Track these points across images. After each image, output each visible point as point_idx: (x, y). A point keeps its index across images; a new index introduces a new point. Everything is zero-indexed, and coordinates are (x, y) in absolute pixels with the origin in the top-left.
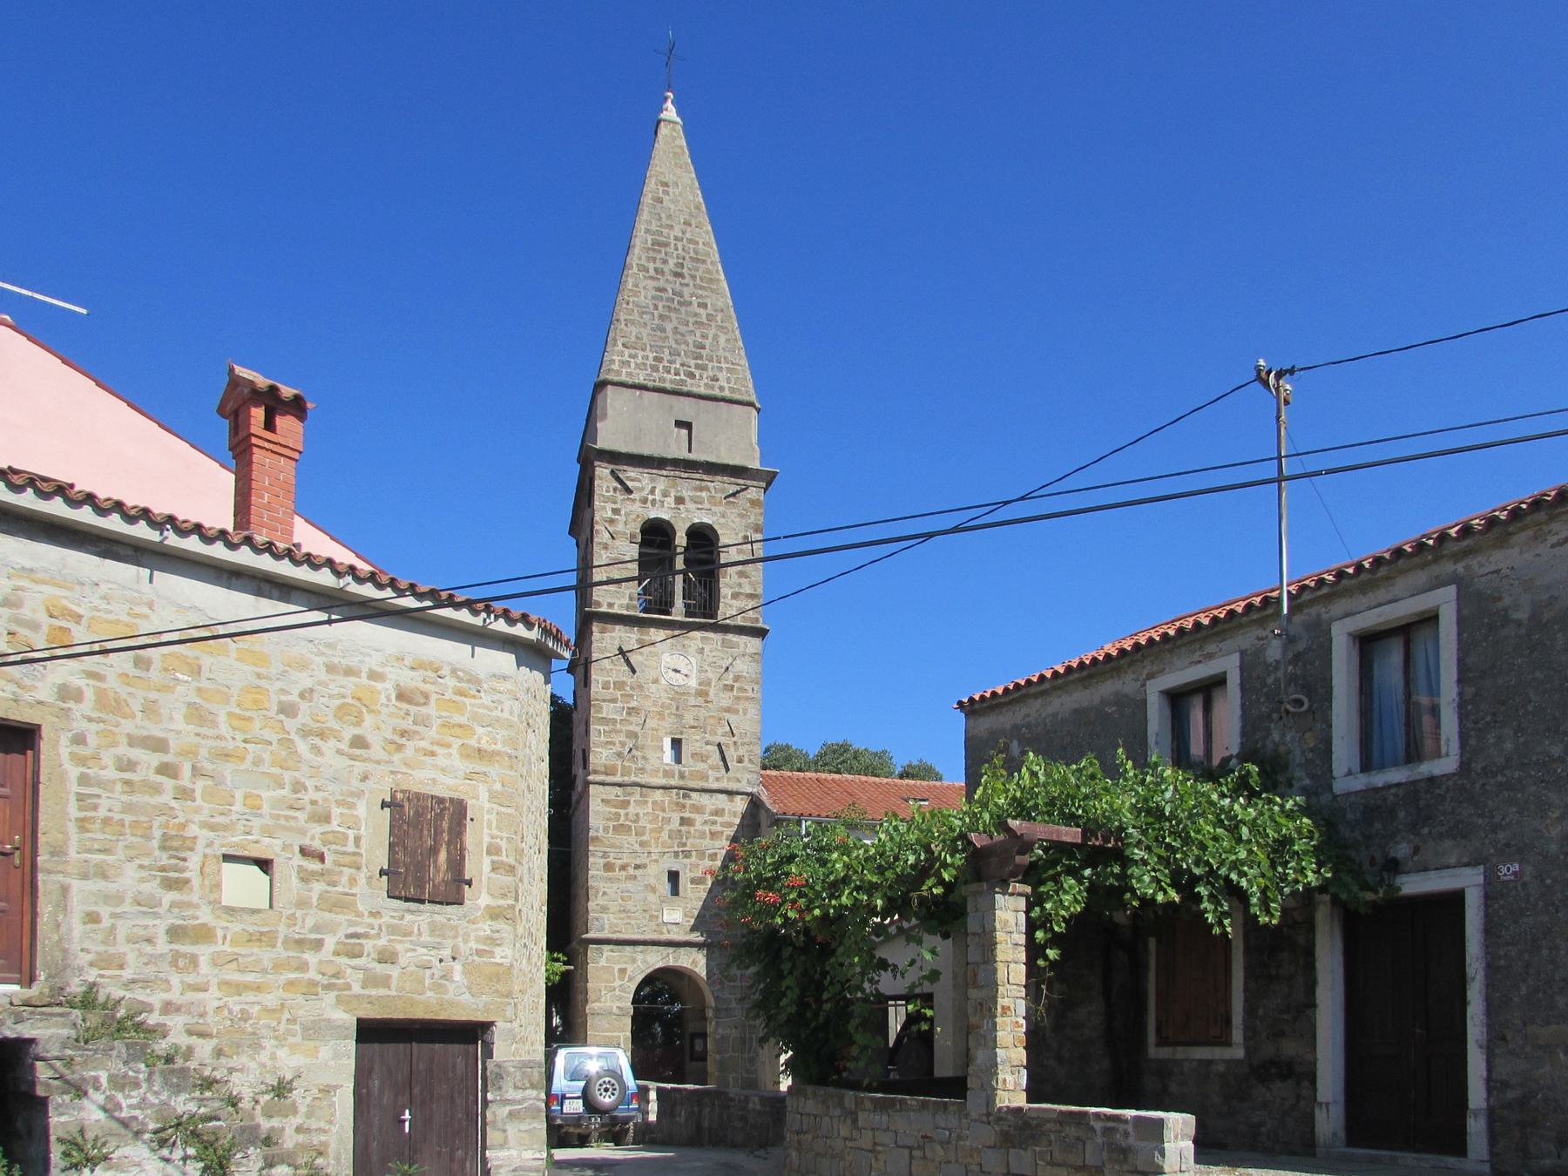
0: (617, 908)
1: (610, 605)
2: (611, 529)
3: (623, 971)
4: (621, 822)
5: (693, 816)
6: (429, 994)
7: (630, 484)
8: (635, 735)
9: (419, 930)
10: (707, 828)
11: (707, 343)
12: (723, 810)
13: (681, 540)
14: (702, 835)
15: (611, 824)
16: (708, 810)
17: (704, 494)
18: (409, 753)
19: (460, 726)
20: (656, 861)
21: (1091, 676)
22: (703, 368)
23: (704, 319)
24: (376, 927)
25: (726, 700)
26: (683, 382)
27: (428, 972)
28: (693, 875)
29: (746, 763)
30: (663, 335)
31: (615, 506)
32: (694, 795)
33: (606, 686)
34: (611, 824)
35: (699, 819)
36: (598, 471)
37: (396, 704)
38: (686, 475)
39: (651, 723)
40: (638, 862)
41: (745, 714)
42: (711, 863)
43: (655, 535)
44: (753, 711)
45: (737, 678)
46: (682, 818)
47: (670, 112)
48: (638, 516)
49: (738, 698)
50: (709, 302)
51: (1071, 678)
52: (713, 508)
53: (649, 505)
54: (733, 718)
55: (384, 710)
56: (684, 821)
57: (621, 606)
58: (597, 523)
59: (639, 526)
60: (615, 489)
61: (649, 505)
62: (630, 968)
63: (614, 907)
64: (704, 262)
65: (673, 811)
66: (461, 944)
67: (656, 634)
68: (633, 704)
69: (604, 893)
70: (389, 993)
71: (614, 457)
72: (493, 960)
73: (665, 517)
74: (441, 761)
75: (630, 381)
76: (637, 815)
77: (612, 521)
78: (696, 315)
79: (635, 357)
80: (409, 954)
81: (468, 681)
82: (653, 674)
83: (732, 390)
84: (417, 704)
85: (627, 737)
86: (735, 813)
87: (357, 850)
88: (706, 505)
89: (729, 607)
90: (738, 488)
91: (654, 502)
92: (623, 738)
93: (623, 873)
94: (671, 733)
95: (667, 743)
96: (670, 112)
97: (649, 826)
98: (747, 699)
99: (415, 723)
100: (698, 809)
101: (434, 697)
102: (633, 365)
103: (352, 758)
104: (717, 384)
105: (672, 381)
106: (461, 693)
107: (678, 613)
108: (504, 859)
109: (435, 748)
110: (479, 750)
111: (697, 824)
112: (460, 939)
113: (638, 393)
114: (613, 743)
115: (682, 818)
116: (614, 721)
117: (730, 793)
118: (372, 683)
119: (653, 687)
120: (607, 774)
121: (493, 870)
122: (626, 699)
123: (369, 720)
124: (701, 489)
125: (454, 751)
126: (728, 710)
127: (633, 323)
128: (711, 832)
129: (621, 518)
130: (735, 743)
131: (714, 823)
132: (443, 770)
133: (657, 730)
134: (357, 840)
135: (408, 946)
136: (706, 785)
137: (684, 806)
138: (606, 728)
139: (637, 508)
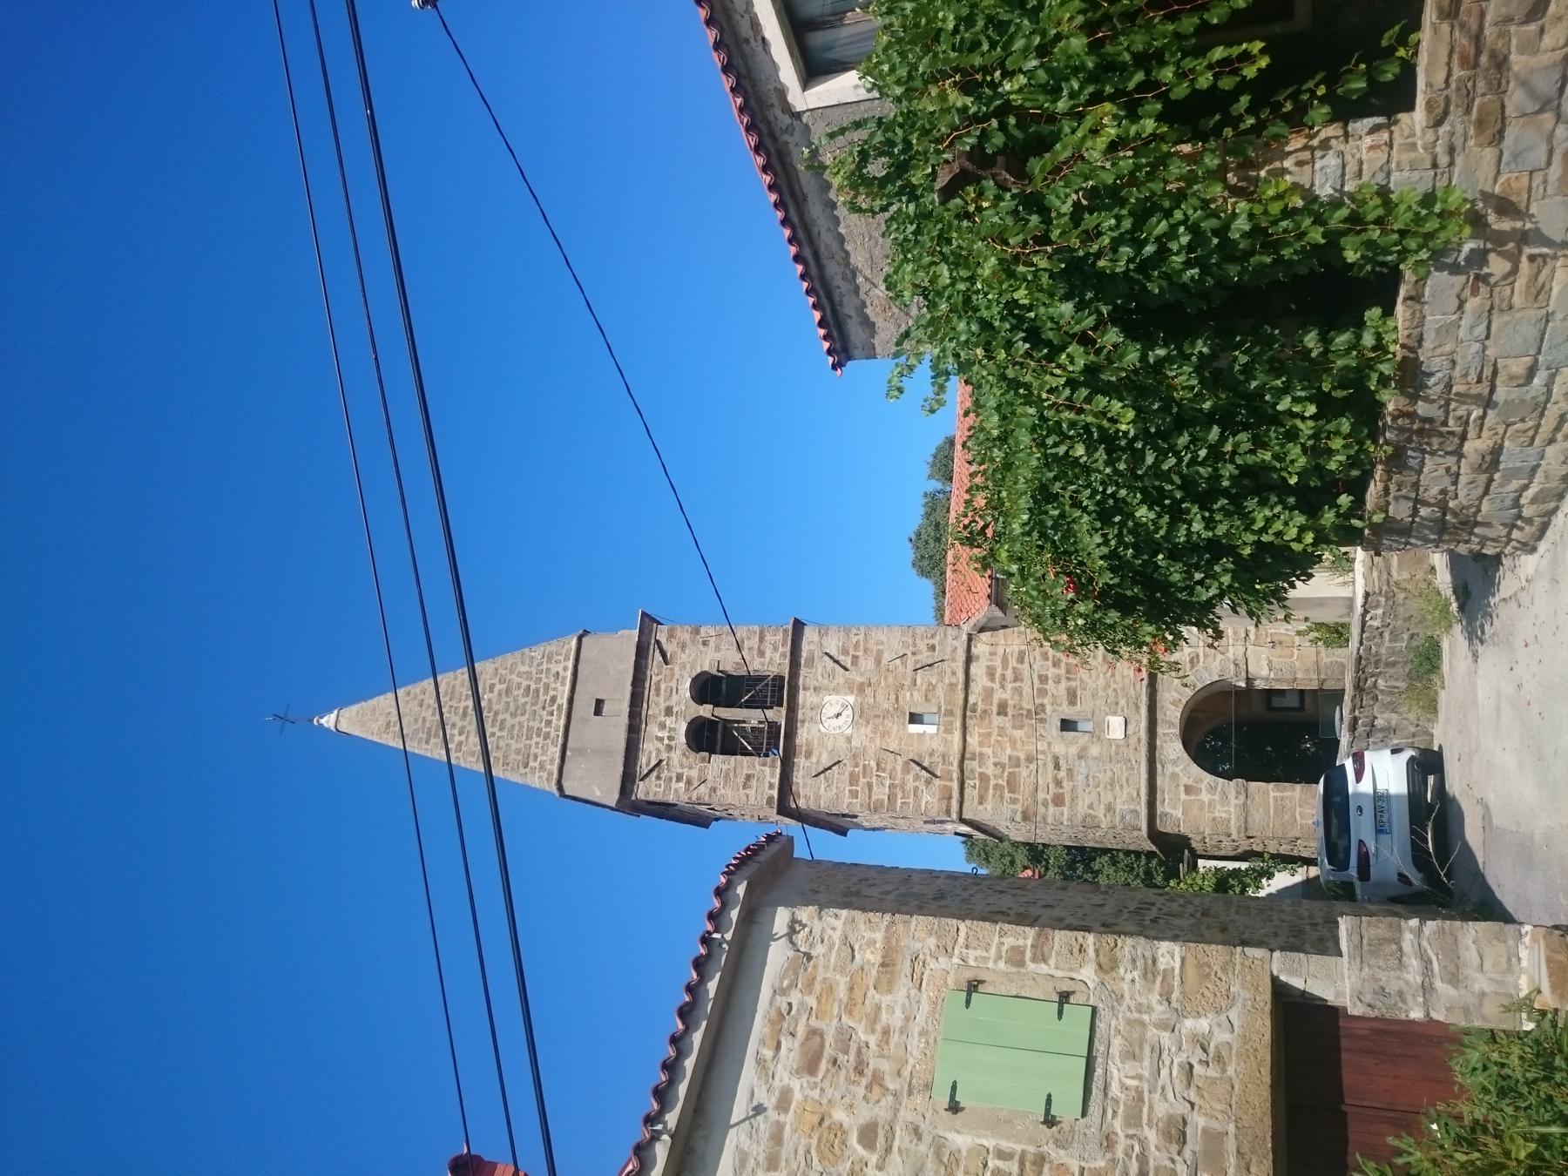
0: (1110, 794)
1: (771, 786)
2: (696, 784)
3: (1188, 790)
4: (1005, 783)
5: (995, 702)
6: (1230, 1071)
7: (653, 763)
8: (906, 764)
9: (1132, 1078)
10: (1009, 686)
11: (525, 683)
12: (988, 667)
13: (706, 711)
14: (1018, 691)
15: (1007, 795)
16: (989, 684)
17: (663, 686)
18: (885, 1066)
19: (851, 989)
20: (1049, 744)
21: (793, 194)
22: (547, 687)
23: (505, 686)
24: (1129, 1142)
25: (867, 664)
26: (560, 707)
27: (1198, 1069)
28: (1065, 703)
29: (935, 641)
30: (517, 728)
31: (674, 779)
32: (972, 700)
33: (854, 794)
34: (1007, 795)
35: (999, 695)
36: (641, 796)
37: (820, 1077)
38: (645, 705)
39: (893, 746)
40: (1051, 765)
41: (883, 643)
42: (1050, 681)
43: (705, 738)
44: (878, 635)
45: (845, 652)
46: (999, 714)
47: (328, 721)
48: (684, 754)
49: (866, 650)
50: (489, 682)
51: (795, 219)
52: (677, 677)
53: (673, 743)
54: (886, 657)
55: (829, 1092)
56: (1002, 710)
57: (772, 775)
58: (690, 798)
59: (693, 754)
60: (658, 778)
61: (673, 743)
62: (1184, 780)
63: (1107, 797)
64: (454, 687)
65: (990, 722)
66: (1154, 1016)
67: (803, 735)
68: (873, 764)
69: (1091, 806)
70: (1231, 1135)
71: (629, 779)
72: (1177, 971)
73: (683, 727)
74: (896, 1020)
75: (557, 761)
76: (996, 765)
77: (689, 782)
78: (500, 694)
79: (536, 757)
80: (1170, 1096)
81: (796, 973)
82: (841, 743)
83: (567, 659)
84: (822, 1046)
85: (908, 773)
86: (991, 654)
87: (1017, 1157)
88: (674, 684)
89: (772, 662)
90: (657, 652)
91: (670, 738)
92: (910, 777)
93: (1065, 784)
94: (903, 724)
95: (915, 729)
96: (328, 721)
97: (1009, 751)
98: (866, 641)
99: (846, 1052)
100: (989, 693)
101: (813, 1022)
102: (544, 758)
103: (888, 1150)
104: (562, 673)
105: (559, 718)
106: (810, 983)
107: (778, 715)
108: (1029, 942)
109: (879, 1028)
110: (883, 965)
111: (1004, 696)
112: (1146, 1017)
113: (568, 753)
114: (916, 789)
115: (999, 714)
116: (892, 786)
117: (969, 659)
118: (793, 1105)
119: (856, 743)
120: (950, 797)
121: (1045, 960)
122: (868, 770)
123: (839, 1115)
124: (658, 689)
125: (886, 1000)
126: (878, 662)
127: (505, 757)
128: (1015, 681)
129: (686, 772)
130: (914, 654)
131: (1003, 676)
132: (907, 1019)
133: (901, 739)
134: (1002, 1155)
135: (1156, 1096)
136: (961, 686)
137: (985, 711)
138: (899, 796)
139: (676, 756)
